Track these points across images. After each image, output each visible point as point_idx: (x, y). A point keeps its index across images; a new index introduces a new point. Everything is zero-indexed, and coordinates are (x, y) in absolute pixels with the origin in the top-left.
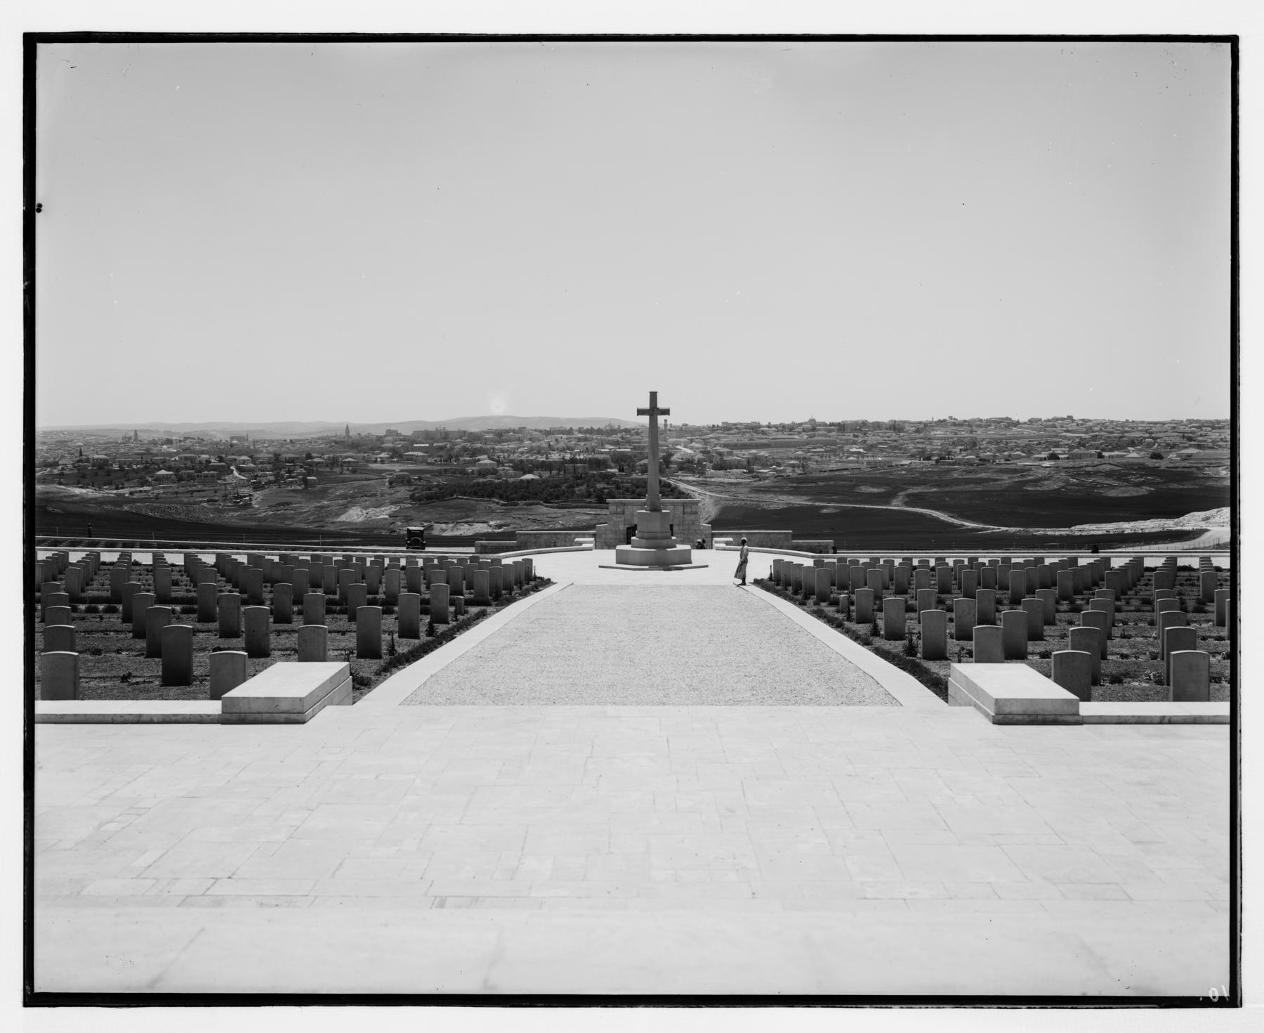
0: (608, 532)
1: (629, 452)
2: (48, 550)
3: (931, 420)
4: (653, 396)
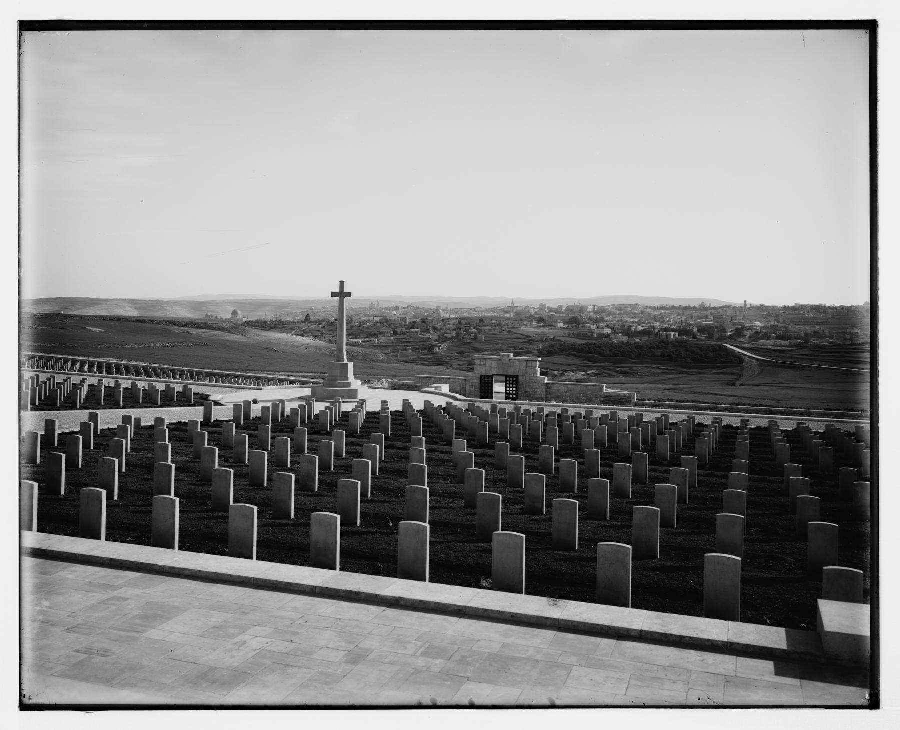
0: (475, 378)
1: (713, 324)
2: (680, 413)
3: (574, 305)
4: (342, 283)
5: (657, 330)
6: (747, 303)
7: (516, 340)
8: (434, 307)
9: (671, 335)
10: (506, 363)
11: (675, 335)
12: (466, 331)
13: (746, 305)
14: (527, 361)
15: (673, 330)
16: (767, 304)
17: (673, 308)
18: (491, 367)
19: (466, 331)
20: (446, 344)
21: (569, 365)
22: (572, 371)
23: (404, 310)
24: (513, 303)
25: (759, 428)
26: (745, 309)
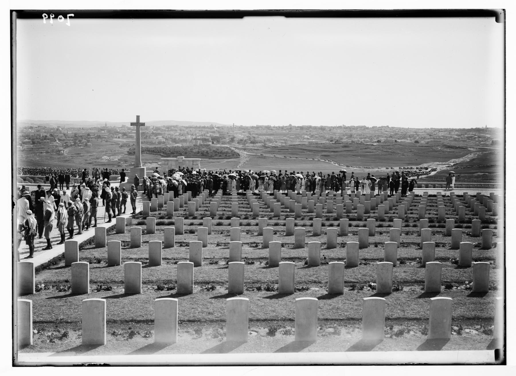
4: (138, 117)
5: (190, 140)
6: (235, 125)
7: (111, 146)
8: (56, 127)
9: (198, 142)
10: (180, 163)
11: (200, 142)
12: (80, 141)
13: (234, 126)
14: (193, 161)
15: (199, 139)
16: (244, 125)
17: (196, 127)
18: (171, 165)
19: (80, 141)
20: (67, 149)
21: (147, 160)
22: (149, 163)
23: (36, 129)
24: (106, 125)
25: (338, 191)
26: (233, 128)
